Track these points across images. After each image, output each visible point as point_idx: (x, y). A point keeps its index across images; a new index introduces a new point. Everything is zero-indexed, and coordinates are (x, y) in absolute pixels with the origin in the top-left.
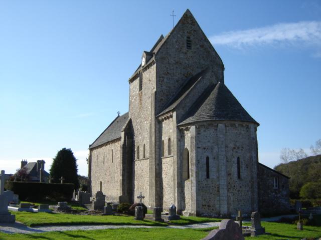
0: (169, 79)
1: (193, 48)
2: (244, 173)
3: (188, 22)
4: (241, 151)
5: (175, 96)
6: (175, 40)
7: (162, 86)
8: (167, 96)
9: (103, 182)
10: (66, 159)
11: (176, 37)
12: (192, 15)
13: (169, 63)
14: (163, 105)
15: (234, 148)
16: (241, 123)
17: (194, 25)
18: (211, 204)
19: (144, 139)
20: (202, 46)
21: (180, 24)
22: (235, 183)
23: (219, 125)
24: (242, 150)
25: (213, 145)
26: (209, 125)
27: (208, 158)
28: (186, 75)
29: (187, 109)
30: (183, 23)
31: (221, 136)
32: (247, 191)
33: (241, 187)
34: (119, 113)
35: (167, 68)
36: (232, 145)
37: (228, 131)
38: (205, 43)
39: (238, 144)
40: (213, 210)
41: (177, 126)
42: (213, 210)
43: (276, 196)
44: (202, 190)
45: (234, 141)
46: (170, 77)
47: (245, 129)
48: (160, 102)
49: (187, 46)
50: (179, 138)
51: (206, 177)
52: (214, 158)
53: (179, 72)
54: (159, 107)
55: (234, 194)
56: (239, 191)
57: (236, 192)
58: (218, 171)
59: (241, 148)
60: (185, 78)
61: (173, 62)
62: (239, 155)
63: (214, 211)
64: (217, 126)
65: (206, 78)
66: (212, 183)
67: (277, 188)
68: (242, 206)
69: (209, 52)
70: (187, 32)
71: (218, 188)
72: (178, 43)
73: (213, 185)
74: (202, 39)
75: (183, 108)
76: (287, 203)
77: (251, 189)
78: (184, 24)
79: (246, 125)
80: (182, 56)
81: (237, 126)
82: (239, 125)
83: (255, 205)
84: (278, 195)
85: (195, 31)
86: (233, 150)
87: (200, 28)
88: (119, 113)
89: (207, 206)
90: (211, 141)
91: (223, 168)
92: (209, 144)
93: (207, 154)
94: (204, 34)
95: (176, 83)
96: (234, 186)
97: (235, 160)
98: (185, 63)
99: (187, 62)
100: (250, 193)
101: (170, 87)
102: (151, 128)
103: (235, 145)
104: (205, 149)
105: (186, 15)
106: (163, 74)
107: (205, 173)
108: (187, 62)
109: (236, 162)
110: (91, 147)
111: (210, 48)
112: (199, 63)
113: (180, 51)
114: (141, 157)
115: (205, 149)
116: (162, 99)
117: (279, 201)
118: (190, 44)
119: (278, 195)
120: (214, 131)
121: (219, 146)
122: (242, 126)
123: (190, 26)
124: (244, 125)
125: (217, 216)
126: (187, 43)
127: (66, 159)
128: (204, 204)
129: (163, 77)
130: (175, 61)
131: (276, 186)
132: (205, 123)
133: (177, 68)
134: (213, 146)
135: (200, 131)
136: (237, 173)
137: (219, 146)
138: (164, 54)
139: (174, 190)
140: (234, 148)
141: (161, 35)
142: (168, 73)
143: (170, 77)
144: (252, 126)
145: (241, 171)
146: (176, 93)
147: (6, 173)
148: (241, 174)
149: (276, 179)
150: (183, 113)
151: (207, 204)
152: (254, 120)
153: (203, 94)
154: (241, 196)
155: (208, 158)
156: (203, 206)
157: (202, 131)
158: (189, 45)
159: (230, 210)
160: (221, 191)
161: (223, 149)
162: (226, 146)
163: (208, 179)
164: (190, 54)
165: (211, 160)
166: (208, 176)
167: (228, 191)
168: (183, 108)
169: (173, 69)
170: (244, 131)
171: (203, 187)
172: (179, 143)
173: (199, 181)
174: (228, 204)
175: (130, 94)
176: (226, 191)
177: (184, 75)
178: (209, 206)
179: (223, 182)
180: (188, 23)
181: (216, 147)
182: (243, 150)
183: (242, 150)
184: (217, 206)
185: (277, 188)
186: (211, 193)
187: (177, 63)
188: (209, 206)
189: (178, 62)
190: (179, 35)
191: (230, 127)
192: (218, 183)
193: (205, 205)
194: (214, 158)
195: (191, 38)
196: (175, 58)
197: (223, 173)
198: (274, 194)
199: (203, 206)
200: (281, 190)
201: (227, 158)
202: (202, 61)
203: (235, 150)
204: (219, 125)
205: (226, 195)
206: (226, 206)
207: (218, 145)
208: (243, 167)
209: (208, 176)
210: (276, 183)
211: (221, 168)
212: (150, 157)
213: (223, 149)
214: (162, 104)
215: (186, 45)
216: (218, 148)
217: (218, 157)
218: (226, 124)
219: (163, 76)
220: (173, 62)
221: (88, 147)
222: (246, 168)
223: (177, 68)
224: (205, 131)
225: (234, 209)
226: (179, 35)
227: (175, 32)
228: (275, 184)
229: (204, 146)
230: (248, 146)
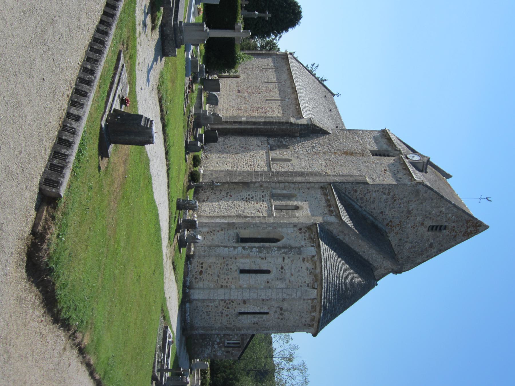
0: (386, 202)
1: (430, 233)
2: (246, 320)
3: (473, 227)
4: (277, 317)
5: (360, 209)
6: (443, 209)
8: (361, 199)
9: (239, 80)
11: (447, 212)
12: (480, 232)
13: (408, 202)
14: (347, 193)
15: (281, 309)
16: (317, 319)
17: (464, 235)
18: (204, 276)
19: (298, 159)
20: (431, 246)
21: (466, 217)
22: (232, 308)
23: (316, 291)
24: (279, 318)
25: (287, 281)
26: (316, 276)
27: (268, 272)
28: (390, 224)
29: (341, 237)
30: (467, 221)
31: (299, 294)
32: (221, 323)
33: (227, 315)
34: (339, 95)
35: (402, 199)
36: (286, 305)
37: (306, 301)
38: (435, 250)
39: (286, 314)
40: (196, 278)
41: (316, 224)
42: (196, 278)
43: (216, 343)
44: (224, 262)
45: (291, 310)
46: (389, 203)
47: (308, 322)
48: (353, 190)
49: (433, 226)
50: (299, 226)
51: (241, 269)
52: (268, 282)
53: (395, 216)
54: (345, 188)
55: (217, 307)
56: (222, 313)
57: (220, 310)
58: (250, 288)
59: (281, 317)
60: (385, 223)
61: (411, 208)
62: (272, 313)
63: (193, 279)
64: (314, 288)
65: (384, 262)
66: (233, 279)
67: (226, 344)
68: (201, 316)
69: (422, 255)
70: (454, 227)
71: (227, 286)
72: (438, 214)
73: (230, 280)
74: (442, 246)
75: (342, 232)
76: (206, 356)
77: (224, 327)
78: (467, 223)
79: (313, 325)
80: (419, 219)
81: (313, 314)
82: (314, 316)
83: (202, 332)
84: (216, 346)
85: (455, 236)
86: (278, 307)
87: (459, 243)
88: (339, 95)
89: (201, 269)
90: (292, 279)
91: (255, 296)
92: (288, 275)
93: (274, 271)
95: (379, 212)
96: (228, 308)
97: (265, 310)
98: (408, 224)
99: (409, 225)
100: (219, 325)
101: (373, 202)
102: (316, 174)
103: (287, 310)
104: (282, 268)
105: (480, 226)
106: (394, 195)
108: (409, 225)
109: (262, 311)
110: (290, 56)
111: (428, 256)
112: (406, 242)
113: (427, 217)
114: (273, 154)
116: (356, 191)
117: (208, 347)
118: (436, 229)
119: (216, 346)
120: (307, 282)
121: (285, 290)
122: (313, 320)
123: (463, 230)
124: (314, 323)
125: (188, 284)
126: (437, 226)
128: (204, 265)
129: (389, 193)
130: (412, 210)
131: (228, 343)
132: (318, 270)
133: (402, 212)
134: (285, 280)
136: (246, 311)
137: (285, 290)
138: (424, 195)
139: (224, 217)
140: (281, 309)
141: (451, 174)
142: (395, 200)
143: (389, 203)
144: (313, 330)
145: (249, 316)
146: (365, 210)
148: (246, 316)
149: (238, 343)
150: (335, 232)
151: (203, 270)
152: (321, 329)
153: (361, 257)
154: (215, 316)
155: (268, 272)
156: (202, 264)
158: (434, 228)
159: (194, 302)
160: (221, 291)
161: (280, 295)
162: (284, 300)
163: (238, 272)
164: (422, 230)
165: (265, 276)
166: (242, 271)
167: (222, 300)
168: (342, 232)
169: (400, 207)
170: (306, 321)
171: (227, 265)
172: (294, 86)
173: (236, 258)
174: (204, 301)
175: (367, 131)
176: (222, 298)
177: (391, 221)
178: (201, 272)
179: (234, 295)
180: (468, 228)
181: (284, 285)
182: (279, 320)
183: (279, 318)
184: (201, 284)
185: (226, 344)
186: (218, 276)
187: (409, 212)
188: (201, 272)
189: (410, 214)
190: (450, 215)
191: (311, 305)
192: (233, 286)
193: (202, 267)
194: (268, 282)
195: (445, 231)
196: (417, 209)
197: (246, 295)
198: (218, 341)
199: (202, 264)
200: (223, 349)
201: (268, 300)
202: (410, 245)
203: (278, 310)
204: (316, 291)
205: (216, 298)
206: (201, 297)
207: (287, 288)
208: (255, 319)
209: (242, 271)
210: (233, 343)
211: (254, 293)
212: (273, 172)
213: (280, 295)
214: (347, 193)
215: (434, 225)
216: (282, 289)
217: (269, 288)
218: (315, 301)
219: (391, 194)
220: (411, 208)
221: (289, 51)
222: (253, 322)
223: (402, 212)
224: (307, 269)
225: (197, 307)
226: (450, 215)
227: (455, 210)
228: (231, 342)
230: (284, 325)
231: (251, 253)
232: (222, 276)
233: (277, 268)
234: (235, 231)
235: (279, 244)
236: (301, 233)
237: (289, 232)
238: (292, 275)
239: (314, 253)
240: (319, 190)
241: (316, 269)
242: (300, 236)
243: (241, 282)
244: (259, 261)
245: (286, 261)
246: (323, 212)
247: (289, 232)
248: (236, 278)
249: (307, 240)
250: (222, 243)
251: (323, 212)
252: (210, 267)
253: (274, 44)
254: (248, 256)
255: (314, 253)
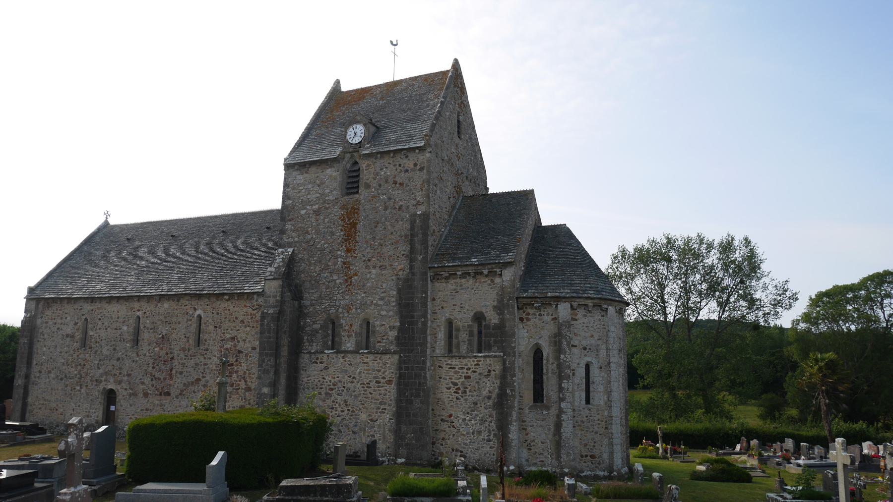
7: (376, 227)
10: (372, 447)
18: (596, 452)
25: (600, 342)
27: (588, 367)
88: (107, 214)
92: (593, 342)
94: (50, 275)
97: (581, 372)
104: (585, 349)
107: (584, 395)
115: (585, 349)
125: (606, 474)
127: (372, 447)
135: (576, 315)
147: (344, 88)
156: (582, 456)
157: (579, 316)
163: (590, 406)
165: (595, 372)
166: (588, 401)
193: (586, 456)
199: (582, 456)
209: (588, 401)
229: (584, 343)
231: (570, 390)
232: (596, 429)
233: (585, 355)
234: (527, 411)
235: (547, 351)
236: (528, 320)
237: (526, 334)
238: (592, 336)
239: (568, 305)
240: (437, 284)
241: (586, 305)
242: (533, 321)
243: (602, 403)
244: (577, 380)
245: (576, 343)
246: (489, 285)
247: (526, 334)
248: (598, 410)
249: (542, 313)
250: (549, 430)
251: (489, 285)
252: (586, 445)
253: (398, 345)
254: (573, 393)
255: (568, 305)
